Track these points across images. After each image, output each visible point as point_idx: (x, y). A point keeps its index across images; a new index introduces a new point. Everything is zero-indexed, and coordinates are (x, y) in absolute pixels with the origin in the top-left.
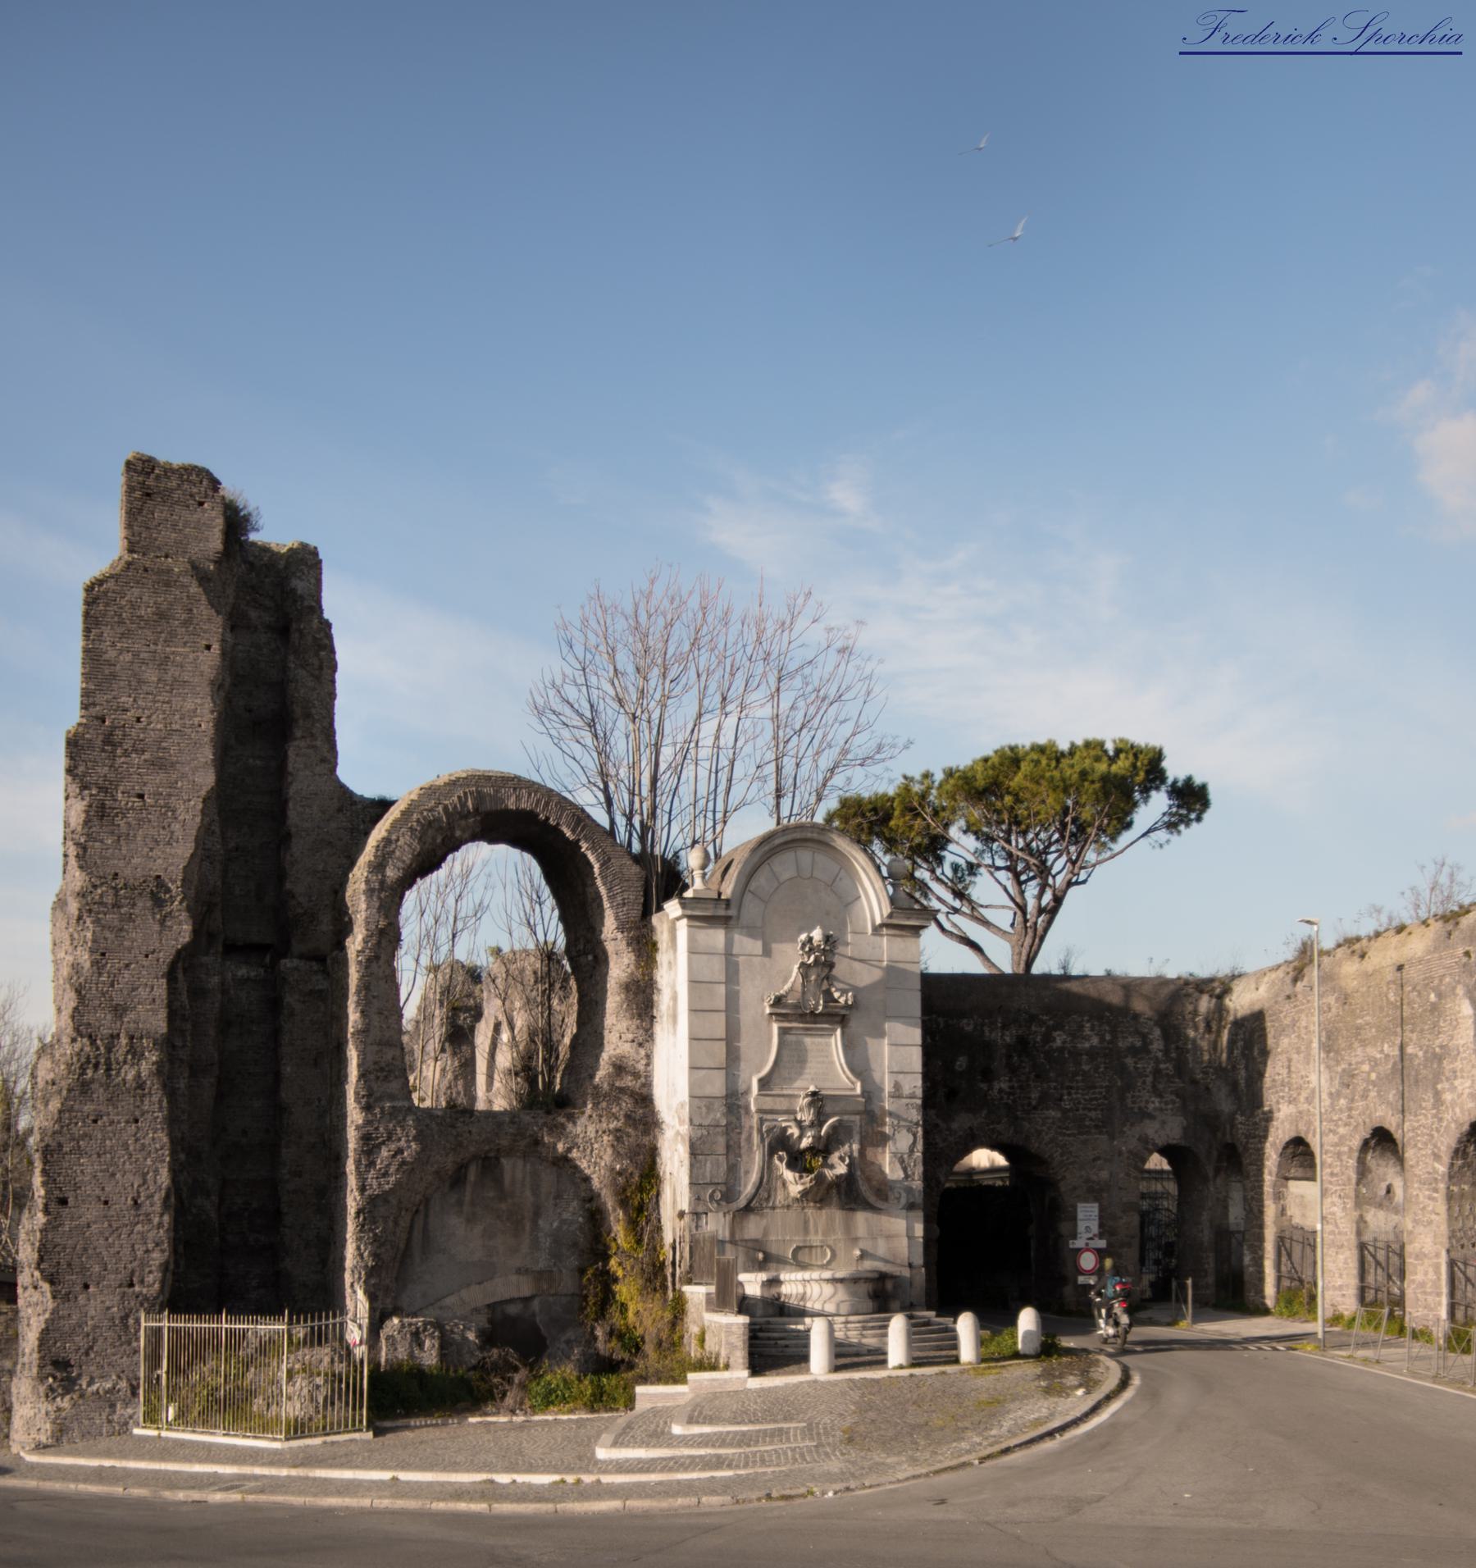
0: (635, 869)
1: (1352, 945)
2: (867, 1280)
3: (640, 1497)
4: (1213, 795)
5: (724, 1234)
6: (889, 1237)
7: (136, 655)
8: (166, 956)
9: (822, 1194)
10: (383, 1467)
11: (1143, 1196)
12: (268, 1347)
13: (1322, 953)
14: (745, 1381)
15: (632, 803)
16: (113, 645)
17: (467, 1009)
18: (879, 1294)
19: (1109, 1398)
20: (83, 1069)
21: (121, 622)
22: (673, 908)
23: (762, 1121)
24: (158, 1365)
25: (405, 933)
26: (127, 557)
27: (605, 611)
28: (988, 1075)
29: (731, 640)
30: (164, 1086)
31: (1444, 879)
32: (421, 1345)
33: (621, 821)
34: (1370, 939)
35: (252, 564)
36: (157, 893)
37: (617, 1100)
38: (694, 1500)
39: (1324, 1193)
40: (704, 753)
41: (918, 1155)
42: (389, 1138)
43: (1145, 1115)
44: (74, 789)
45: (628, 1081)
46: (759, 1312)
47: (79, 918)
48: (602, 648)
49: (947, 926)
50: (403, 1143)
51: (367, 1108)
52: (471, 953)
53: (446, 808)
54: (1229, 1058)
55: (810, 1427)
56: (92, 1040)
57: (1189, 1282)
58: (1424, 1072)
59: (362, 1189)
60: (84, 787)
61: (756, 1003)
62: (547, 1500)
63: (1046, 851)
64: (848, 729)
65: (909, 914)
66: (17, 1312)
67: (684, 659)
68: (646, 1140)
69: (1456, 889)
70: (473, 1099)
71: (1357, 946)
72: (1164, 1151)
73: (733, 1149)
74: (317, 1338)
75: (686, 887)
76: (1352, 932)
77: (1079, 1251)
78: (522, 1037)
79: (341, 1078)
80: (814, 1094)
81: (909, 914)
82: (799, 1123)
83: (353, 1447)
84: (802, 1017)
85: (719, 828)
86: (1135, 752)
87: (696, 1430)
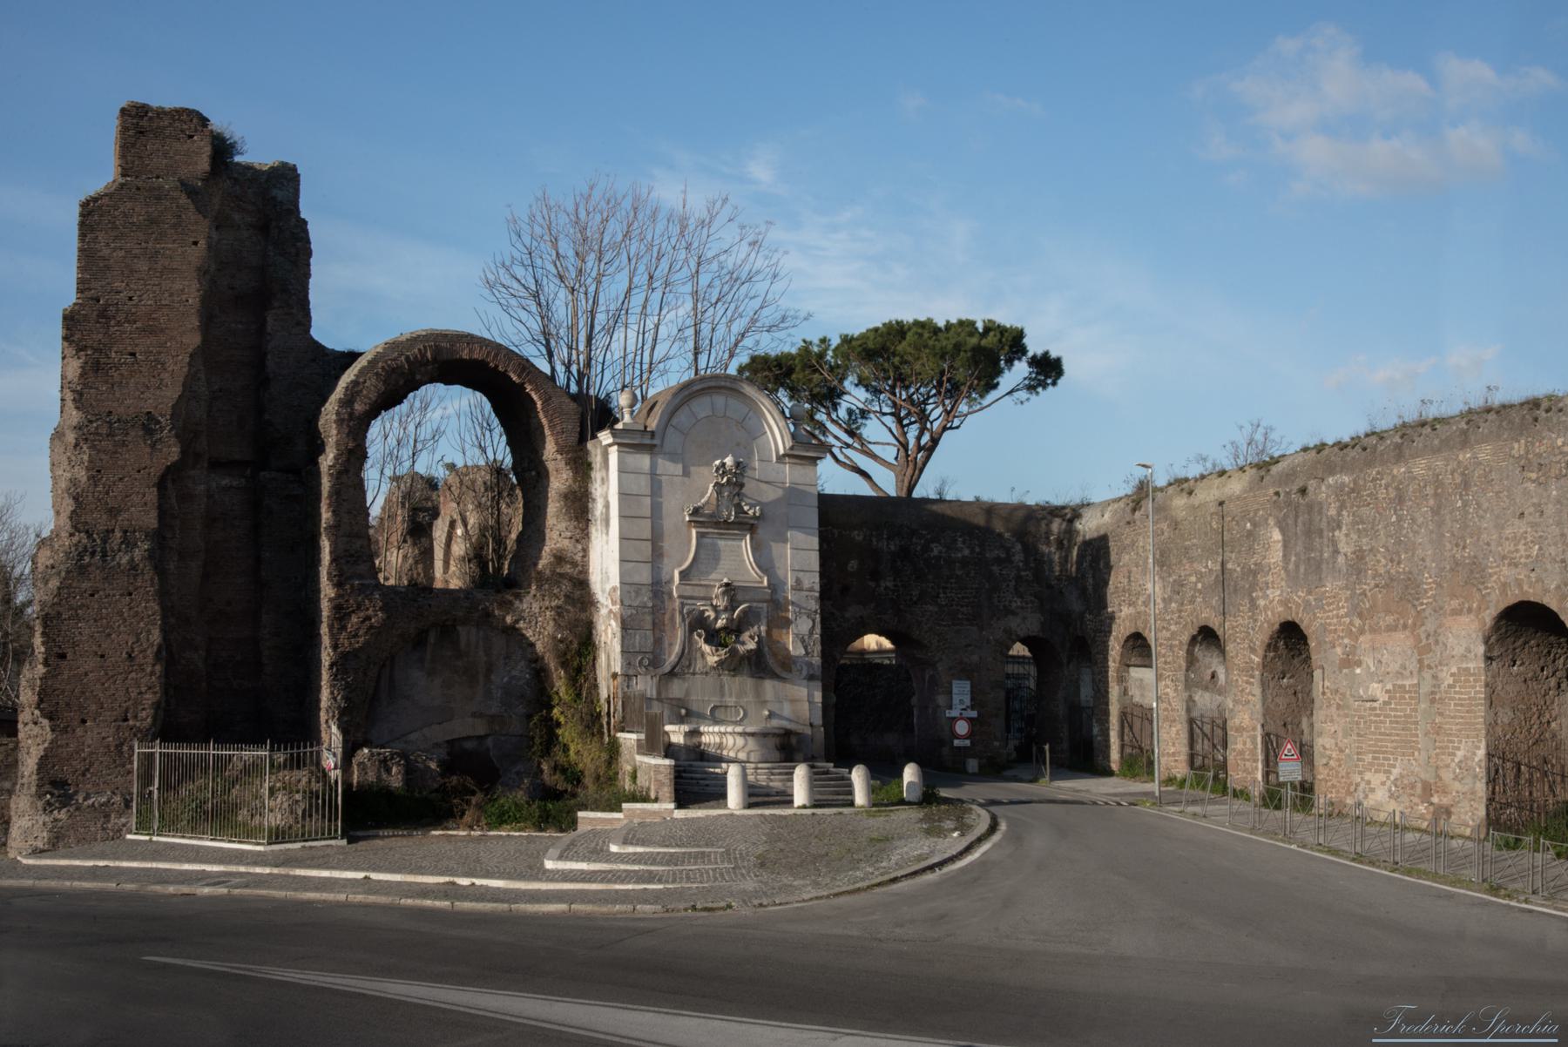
0: (573, 405)
1: (1181, 484)
2: (774, 735)
3: (583, 902)
4: (1066, 366)
5: (652, 692)
6: (793, 701)
7: (128, 252)
8: (156, 471)
9: (735, 664)
10: (357, 869)
11: (1008, 676)
12: (252, 770)
13: (1156, 489)
14: (672, 812)
15: (570, 355)
16: (108, 245)
17: (426, 510)
18: (786, 747)
19: (980, 840)
20: (81, 556)
21: (115, 228)
22: (605, 437)
23: (683, 605)
24: (151, 783)
25: (370, 452)
26: (121, 180)
27: (549, 209)
28: (876, 575)
29: (658, 232)
30: (156, 568)
31: (1259, 437)
32: (388, 771)
33: (560, 369)
34: (1196, 480)
35: (236, 180)
36: (149, 425)
37: (558, 583)
38: (630, 907)
39: (1159, 678)
40: (632, 319)
41: (817, 636)
42: (359, 608)
43: (1009, 612)
44: (71, 351)
45: (567, 569)
46: (683, 757)
47: (76, 445)
48: (547, 238)
49: (841, 457)
50: (370, 612)
51: (338, 586)
52: (429, 467)
53: (407, 358)
54: (1078, 569)
55: (727, 852)
56: (89, 535)
57: (1047, 747)
58: (1242, 583)
59: (335, 647)
60: (79, 350)
61: (677, 510)
62: (502, 901)
63: (925, 402)
64: (756, 303)
65: (808, 448)
66: (18, 743)
67: (616, 247)
68: (583, 616)
69: (1269, 445)
70: (432, 579)
71: (1185, 485)
72: (1024, 641)
73: (658, 626)
74: (295, 763)
75: (617, 421)
76: (1182, 474)
77: (954, 720)
78: (474, 532)
79: (316, 561)
80: (727, 585)
81: (808, 448)
82: (715, 608)
83: (329, 851)
84: (717, 525)
85: (645, 376)
86: (1002, 330)
87: (631, 849)
